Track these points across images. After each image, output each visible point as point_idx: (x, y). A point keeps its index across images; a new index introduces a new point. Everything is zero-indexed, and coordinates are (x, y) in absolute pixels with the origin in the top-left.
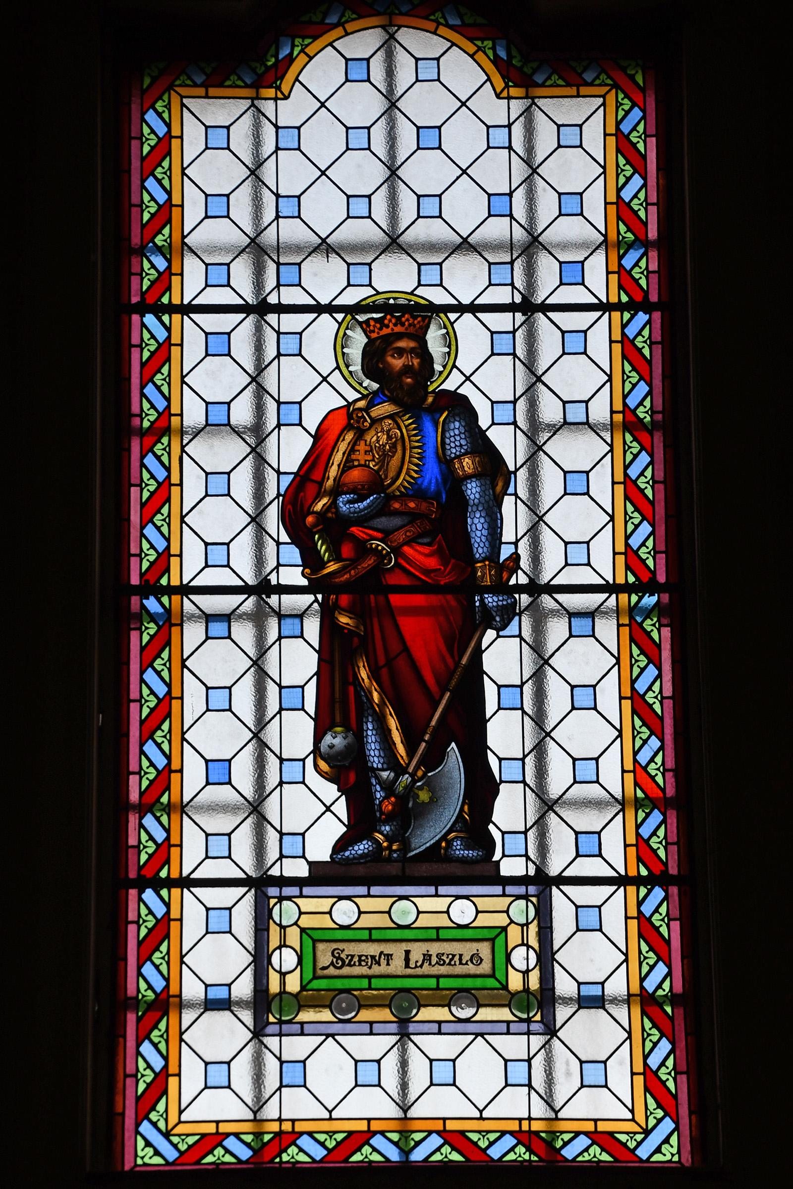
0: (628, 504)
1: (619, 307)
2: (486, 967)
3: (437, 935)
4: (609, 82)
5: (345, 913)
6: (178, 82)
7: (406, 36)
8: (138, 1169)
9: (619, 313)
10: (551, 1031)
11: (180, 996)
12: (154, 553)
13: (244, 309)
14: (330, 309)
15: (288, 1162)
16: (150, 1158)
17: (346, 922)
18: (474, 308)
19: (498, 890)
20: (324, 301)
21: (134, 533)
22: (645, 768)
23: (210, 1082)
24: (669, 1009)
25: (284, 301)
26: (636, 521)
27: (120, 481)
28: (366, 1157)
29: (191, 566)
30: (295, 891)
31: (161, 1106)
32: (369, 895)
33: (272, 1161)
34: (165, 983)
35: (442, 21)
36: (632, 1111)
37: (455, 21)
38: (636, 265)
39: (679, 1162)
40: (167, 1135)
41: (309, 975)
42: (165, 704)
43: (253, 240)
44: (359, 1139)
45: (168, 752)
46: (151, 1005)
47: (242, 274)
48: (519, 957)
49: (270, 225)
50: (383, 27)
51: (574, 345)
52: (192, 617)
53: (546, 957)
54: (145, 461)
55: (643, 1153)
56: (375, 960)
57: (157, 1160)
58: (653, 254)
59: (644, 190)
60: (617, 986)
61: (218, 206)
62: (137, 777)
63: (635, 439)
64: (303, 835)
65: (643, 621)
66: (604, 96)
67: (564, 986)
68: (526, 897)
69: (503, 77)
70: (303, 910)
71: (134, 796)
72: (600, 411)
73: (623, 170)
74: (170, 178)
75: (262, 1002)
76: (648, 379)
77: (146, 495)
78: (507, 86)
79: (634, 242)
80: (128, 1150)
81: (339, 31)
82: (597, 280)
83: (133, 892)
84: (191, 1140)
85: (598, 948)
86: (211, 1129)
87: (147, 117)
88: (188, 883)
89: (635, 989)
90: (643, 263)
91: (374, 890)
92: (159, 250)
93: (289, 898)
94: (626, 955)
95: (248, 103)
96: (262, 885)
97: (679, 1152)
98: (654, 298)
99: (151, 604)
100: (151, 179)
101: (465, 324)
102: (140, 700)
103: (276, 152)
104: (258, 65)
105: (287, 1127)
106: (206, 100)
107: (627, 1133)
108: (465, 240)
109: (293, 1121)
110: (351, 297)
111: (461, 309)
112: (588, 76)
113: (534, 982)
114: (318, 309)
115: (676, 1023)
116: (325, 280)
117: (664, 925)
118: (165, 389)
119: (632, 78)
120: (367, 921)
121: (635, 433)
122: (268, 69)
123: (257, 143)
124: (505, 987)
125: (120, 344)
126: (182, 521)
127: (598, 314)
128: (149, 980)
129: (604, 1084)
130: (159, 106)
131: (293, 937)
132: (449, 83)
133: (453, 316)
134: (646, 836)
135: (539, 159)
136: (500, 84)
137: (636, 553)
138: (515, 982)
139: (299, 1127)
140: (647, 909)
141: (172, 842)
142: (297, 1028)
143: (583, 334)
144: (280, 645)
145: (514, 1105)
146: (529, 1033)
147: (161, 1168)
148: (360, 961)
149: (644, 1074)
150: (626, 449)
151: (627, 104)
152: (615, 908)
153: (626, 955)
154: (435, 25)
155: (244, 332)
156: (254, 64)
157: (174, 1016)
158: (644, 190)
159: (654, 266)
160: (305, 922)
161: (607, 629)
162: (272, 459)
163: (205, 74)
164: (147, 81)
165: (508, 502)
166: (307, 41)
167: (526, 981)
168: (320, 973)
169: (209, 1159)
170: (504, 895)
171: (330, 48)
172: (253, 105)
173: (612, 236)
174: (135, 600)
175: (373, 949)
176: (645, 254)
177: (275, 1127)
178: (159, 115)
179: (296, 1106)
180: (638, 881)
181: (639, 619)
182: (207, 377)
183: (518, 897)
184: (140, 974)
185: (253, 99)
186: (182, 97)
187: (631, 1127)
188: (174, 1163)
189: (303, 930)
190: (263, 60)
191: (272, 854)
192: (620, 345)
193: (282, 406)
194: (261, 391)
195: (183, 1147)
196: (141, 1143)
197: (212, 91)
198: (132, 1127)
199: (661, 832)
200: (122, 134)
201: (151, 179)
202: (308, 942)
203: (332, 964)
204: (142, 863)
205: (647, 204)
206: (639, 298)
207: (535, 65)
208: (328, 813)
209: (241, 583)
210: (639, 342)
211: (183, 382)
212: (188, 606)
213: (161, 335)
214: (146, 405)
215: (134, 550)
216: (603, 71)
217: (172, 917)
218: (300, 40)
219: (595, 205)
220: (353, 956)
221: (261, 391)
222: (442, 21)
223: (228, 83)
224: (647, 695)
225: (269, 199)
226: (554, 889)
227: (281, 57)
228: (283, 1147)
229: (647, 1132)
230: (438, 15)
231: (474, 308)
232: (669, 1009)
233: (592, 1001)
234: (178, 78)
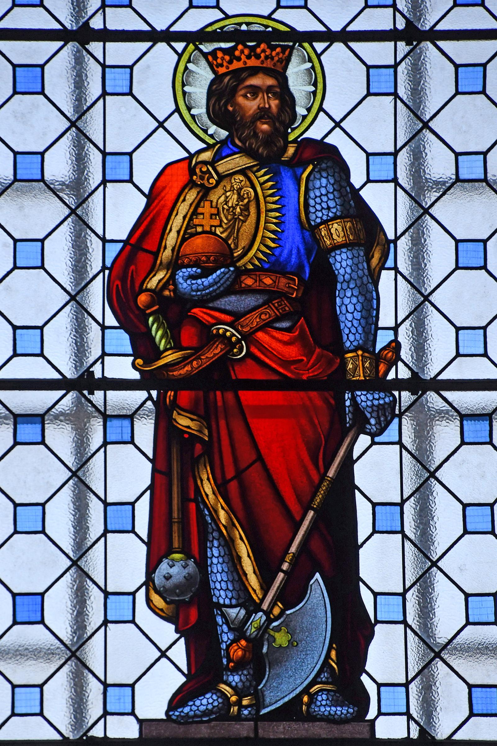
13: (62, 35)
14: (169, 36)
18: (346, 36)
20: (160, 26)
25: (111, 26)
101: (336, 56)
110: (194, 22)
111: (330, 36)
114: (153, 36)
133: (319, 46)
144: (105, 452)
162: (96, 224)
191: (94, 710)
231: (346, 36)
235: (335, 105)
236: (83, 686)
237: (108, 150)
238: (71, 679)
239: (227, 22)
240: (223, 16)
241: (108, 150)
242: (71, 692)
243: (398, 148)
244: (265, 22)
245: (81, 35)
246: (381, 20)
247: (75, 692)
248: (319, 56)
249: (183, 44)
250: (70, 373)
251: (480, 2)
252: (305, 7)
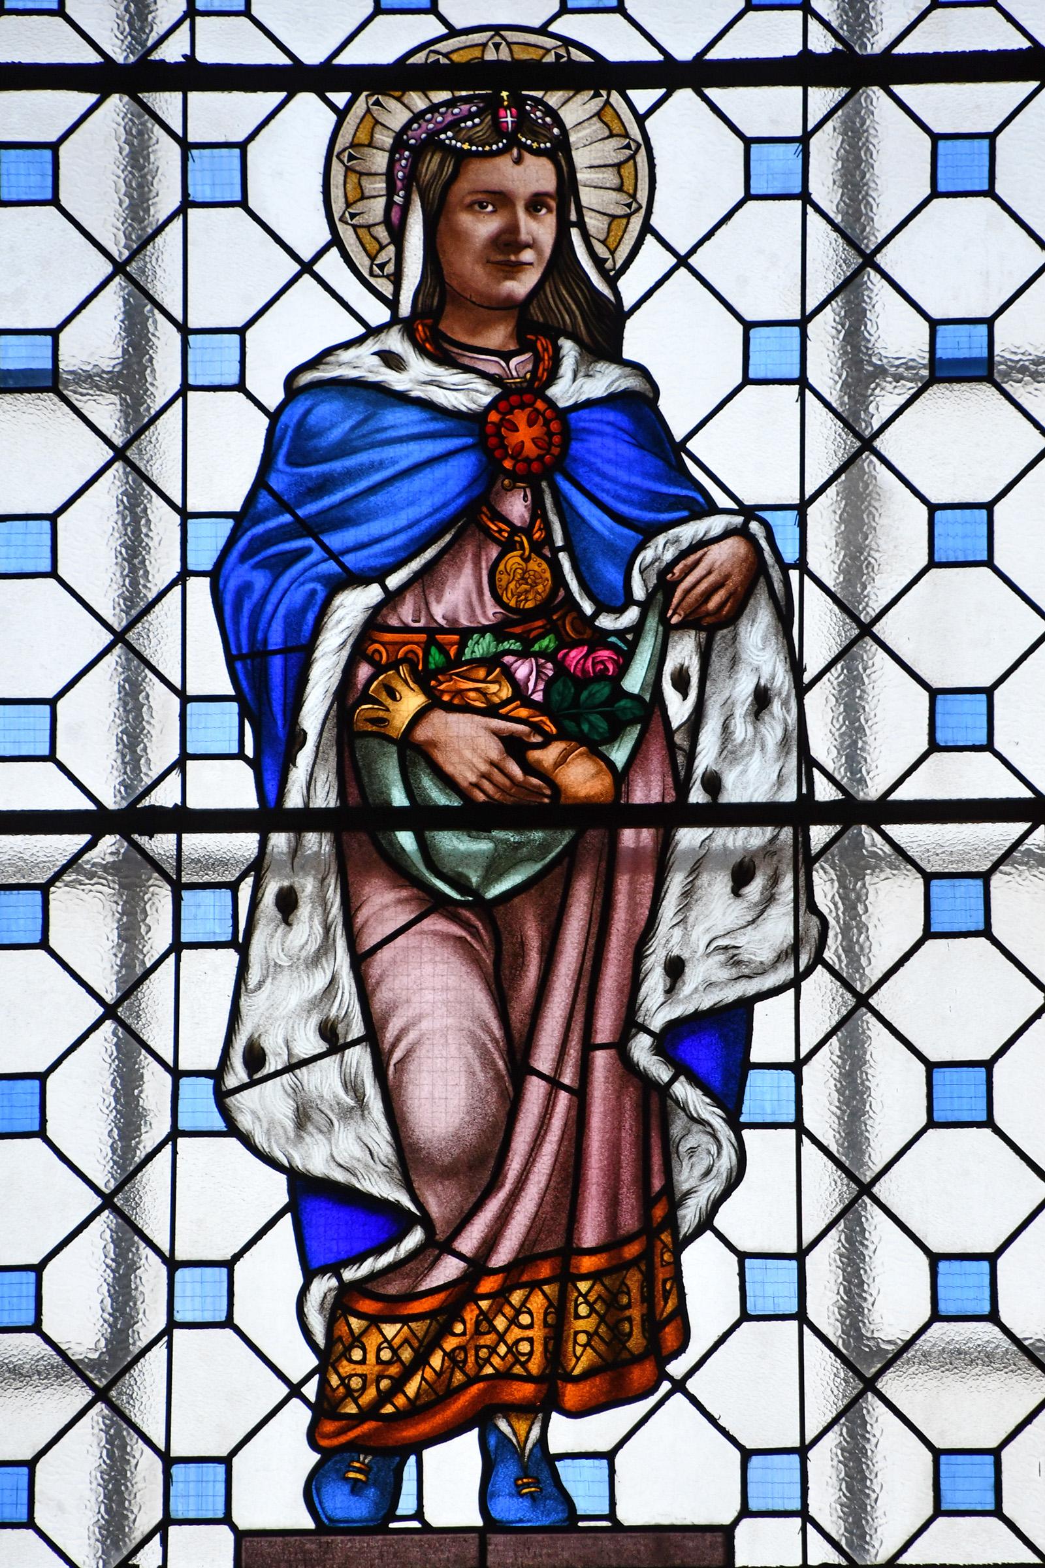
13: (99, 78)
18: (703, 74)
25: (205, 55)
64: (226, 1461)
101: (681, 128)
110: (386, 43)
111: (669, 74)
114: (291, 78)
123: (134, 553)
129: (984, 557)
133: (643, 98)
135: (878, 1156)
191: (826, 148)
194: (141, 301)
221: (141, 301)
231: (703, 74)
235: (677, 218)
236: (866, 1478)
237: (794, 1324)
238: (840, 1462)
240: (444, 31)
241: (794, 1324)
242: (841, 1490)
243: (808, 312)
245: (132, 77)
246: (775, 35)
247: (107, 1512)
248: (641, 119)
249: (346, 96)
251: (55, 6)
252: (247, 13)
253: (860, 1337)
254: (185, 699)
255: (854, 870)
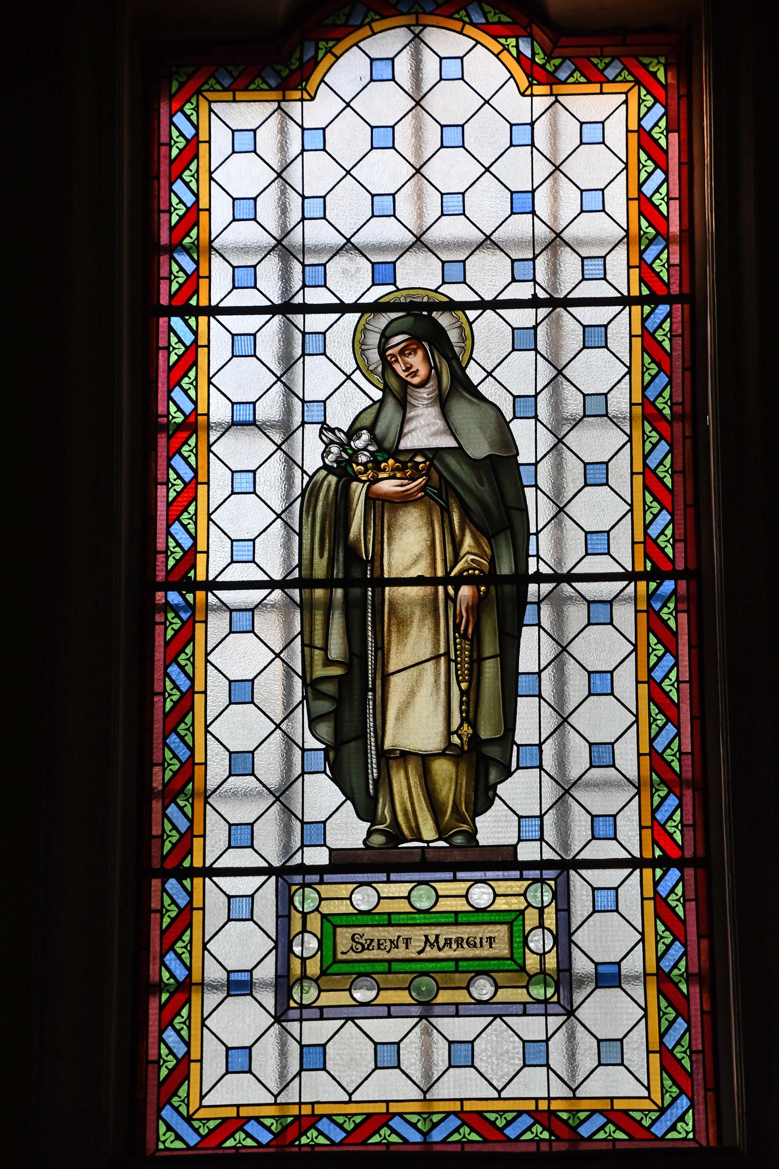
0: (647, 494)
1: (640, 300)
2: (501, 949)
3: (456, 919)
4: (630, 78)
5: (364, 899)
6: (206, 87)
7: (432, 35)
8: (158, 1154)
9: (650, 870)
10: (570, 1013)
11: (208, 415)
12: (184, 385)
13: (271, 310)
15: (307, 1145)
16: (172, 1142)
17: (363, 907)
18: (495, 305)
19: (516, 874)
21: (158, 674)
22: (663, 826)
23: (235, 1060)
24: (683, 987)
25: (309, 301)
26: (655, 511)
27: (147, 481)
28: (385, 1138)
29: (216, 562)
30: (316, 878)
31: (182, 1092)
32: (388, 881)
33: (292, 1144)
34: (193, 406)
35: (466, 19)
36: (648, 1088)
37: (479, 19)
38: (658, 257)
39: (694, 1139)
40: (189, 1119)
41: (329, 960)
42: (191, 352)
43: (279, 242)
44: (380, 1119)
45: (195, 328)
46: (179, 425)
47: (269, 276)
48: (536, 942)
49: (296, 158)
50: (408, 27)
51: (595, 338)
52: (217, 610)
53: (564, 938)
54: (173, 395)
55: (658, 1130)
56: (394, 944)
57: (179, 1145)
58: (675, 248)
59: (665, 184)
60: (633, 965)
61: (245, 209)
62: (163, 627)
63: (654, 429)
65: (661, 609)
66: (626, 93)
67: (581, 966)
68: (542, 881)
69: (528, 76)
70: (323, 896)
71: (157, 785)
72: (619, 402)
73: (649, 437)
74: (197, 181)
75: (283, 984)
76: (682, 938)
77: (172, 494)
78: (531, 85)
79: (655, 237)
80: (150, 1135)
81: (366, 31)
82: (620, 275)
83: (163, 321)
84: (212, 1124)
85: (615, 929)
86: (232, 1113)
87: (175, 119)
88: (214, 311)
89: (652, 968)
90: (664, 256)
91: (393, 876)
92: (187, 251)
93: (310, 885)
94: (631, 505)
95: (275, 105)
96: (287, 875)
97: (694, 1130)
98: (675, 289)
99: (174, 597)
100: (177, 457)
102: (166, 552)
103: (302, 153)
104: (283, 68)
105: (306, 1110)
106: (234, 104)
107: (641, 1111)
108: (488, 237)
109: (313, 1104)
111: (483, 305)
112: (610, 73)
113: (551, 962)
114: (341, 308)
115: (692, 1002)
116: (351, 281)
117: (680, 905)
118: (193, 185)
119: (654, 75)
120: (386, 907)
121: (655, 424)
122: (292, 72)
123: (284, 210)
124: (523, 968)
125: (148, 345)
126: (205, 948)
127: (627, 871)
128: (177, 406)
130: (188, 108)
131: (314, 923)
132: (476, 73)
133: (472, 314)
134: (653, 466)
136: (524, 82)
137: (654, 472)
138: (532, 963)
139: (319, 1110)
140: (663, 890)
141: (201, 207)
142: (316, 1013)
143: (609, 621)
145: (533, 1084)
146: (546, 1015)
147: (184, 1153)
148: (379, 944)
149: (653, 899)
150: (645, 438)
151: (650, 100)
152: (632, 889)
153: (637, 716)
154: (461, 24)
155: (270, 333)
156: (278, 67)
157: (202, 435)
158: (665, 184)
159: (675, 260)
160: (326, 908)
161: (625, 615)
163: (232, 76)
164: (175, 86)
165: (528, 635)
166: (331, 44)
167: (542, 962)
168: (340, 957)
169: (230, 1143)
170: (521, 879)
171: (355, 48)
172: (279, 107)
173: (634, 231)
174: (159, 595)
175: (392, 933)
176: (667, 247)
177: (295, 1110)
178: (188, 117)
179: (318, 1088)
180: (653, 863)
181: (657, 606)
182: (232, 371)
183: (535, 881)
184: (161, 1040)
185: (279, 102)
186: (210, 102)
187: (647, 1105)
188: (195, 1147)
189: (324, 916)
190: (286, 63)
192: (645, 614)
193: (307, 268)
195: (204, 1131)
196: (162, 1128)
197: (239, 95)
198: (160, 741)
199: (677, 817)
200: (149, 137)
201: (177, 457)
202: (328, 927)
203: (352, 948)
204: (161, 1079)
205: (669, 199)
206: (662, 292)
207: (557, 62)
208: (349, 381)
209: (266, 578)
210: (659, 335)
211: (210, 383)
212: (212, 599)
213: (188, 338)
214: (172, 543)
215: (162, 343)
216: (625, 68)
217: (195, 906)
218: (324, 43)
219: (617, 199)
220: (372, 941)
221: (289, 390)
222: (466, 19)
223: (252, 87)
224: (670, 898)
225: (295, 201)
226: (572, 872)
227: (306, 58)
228: (303, 1129)
229: (662, 1110)
230: (463, 13)
231: (495, 305)
232: (683, 987)
233: (608, 977)
234: (206, 82)
237: (537, 628)
239: (398, 294)
244: (433, 294)
250: (276, 863)
253: (565, 775)
254: (304, 197)
255: (559, 604)
